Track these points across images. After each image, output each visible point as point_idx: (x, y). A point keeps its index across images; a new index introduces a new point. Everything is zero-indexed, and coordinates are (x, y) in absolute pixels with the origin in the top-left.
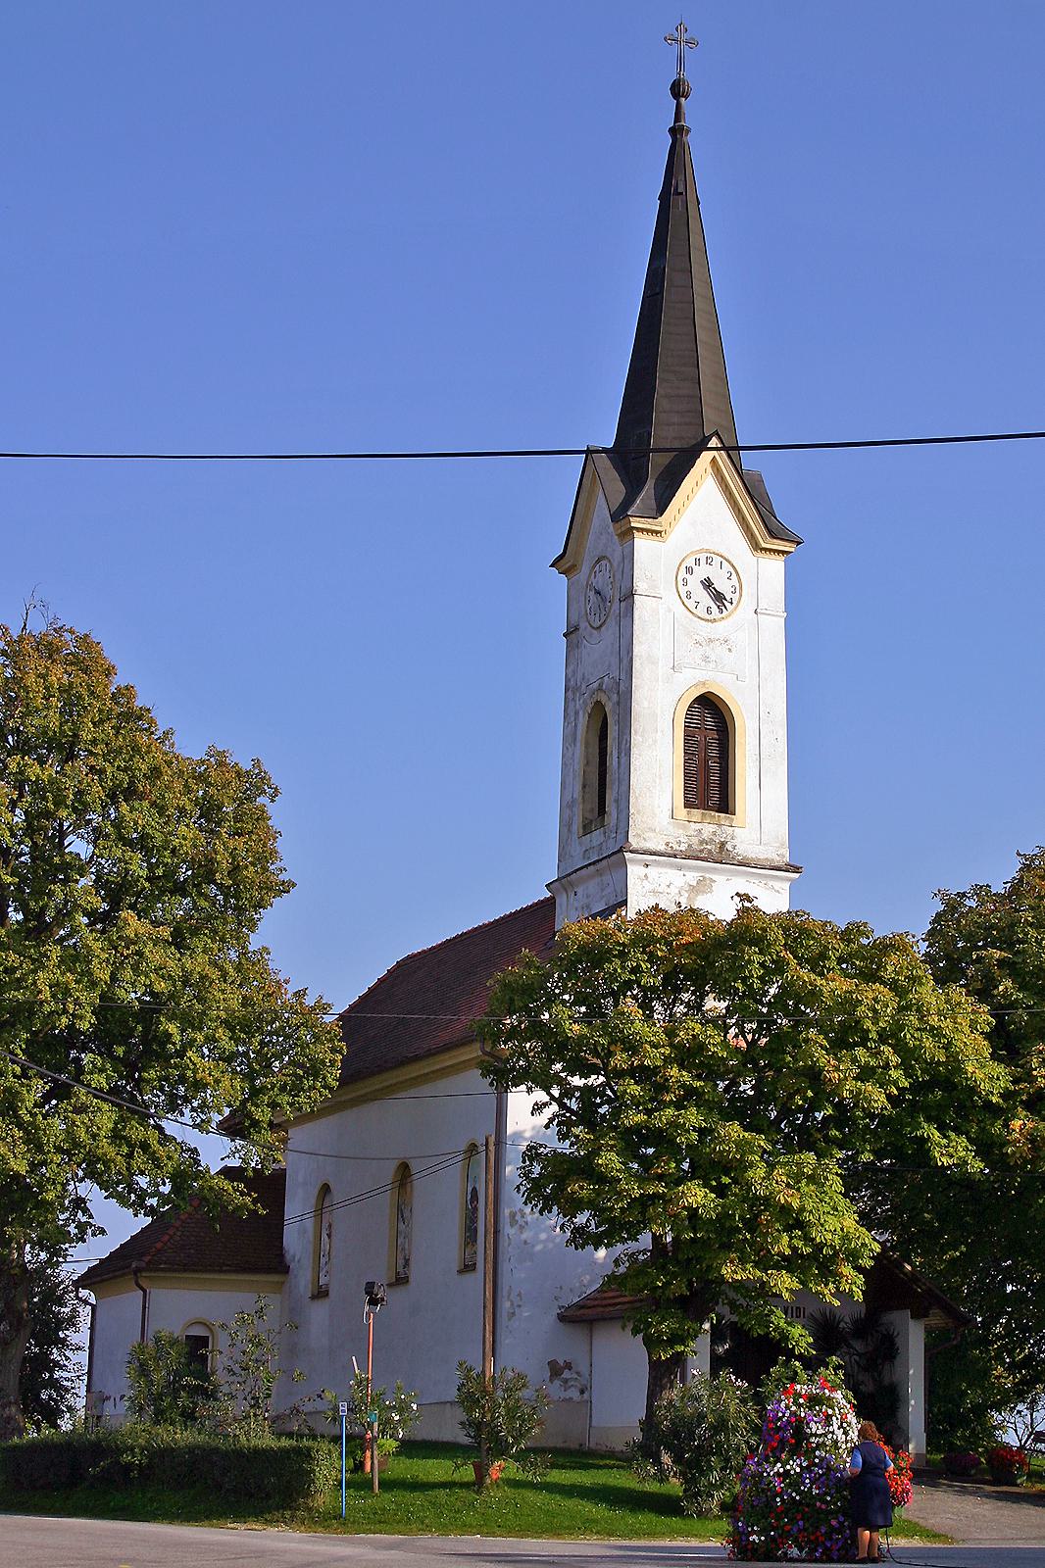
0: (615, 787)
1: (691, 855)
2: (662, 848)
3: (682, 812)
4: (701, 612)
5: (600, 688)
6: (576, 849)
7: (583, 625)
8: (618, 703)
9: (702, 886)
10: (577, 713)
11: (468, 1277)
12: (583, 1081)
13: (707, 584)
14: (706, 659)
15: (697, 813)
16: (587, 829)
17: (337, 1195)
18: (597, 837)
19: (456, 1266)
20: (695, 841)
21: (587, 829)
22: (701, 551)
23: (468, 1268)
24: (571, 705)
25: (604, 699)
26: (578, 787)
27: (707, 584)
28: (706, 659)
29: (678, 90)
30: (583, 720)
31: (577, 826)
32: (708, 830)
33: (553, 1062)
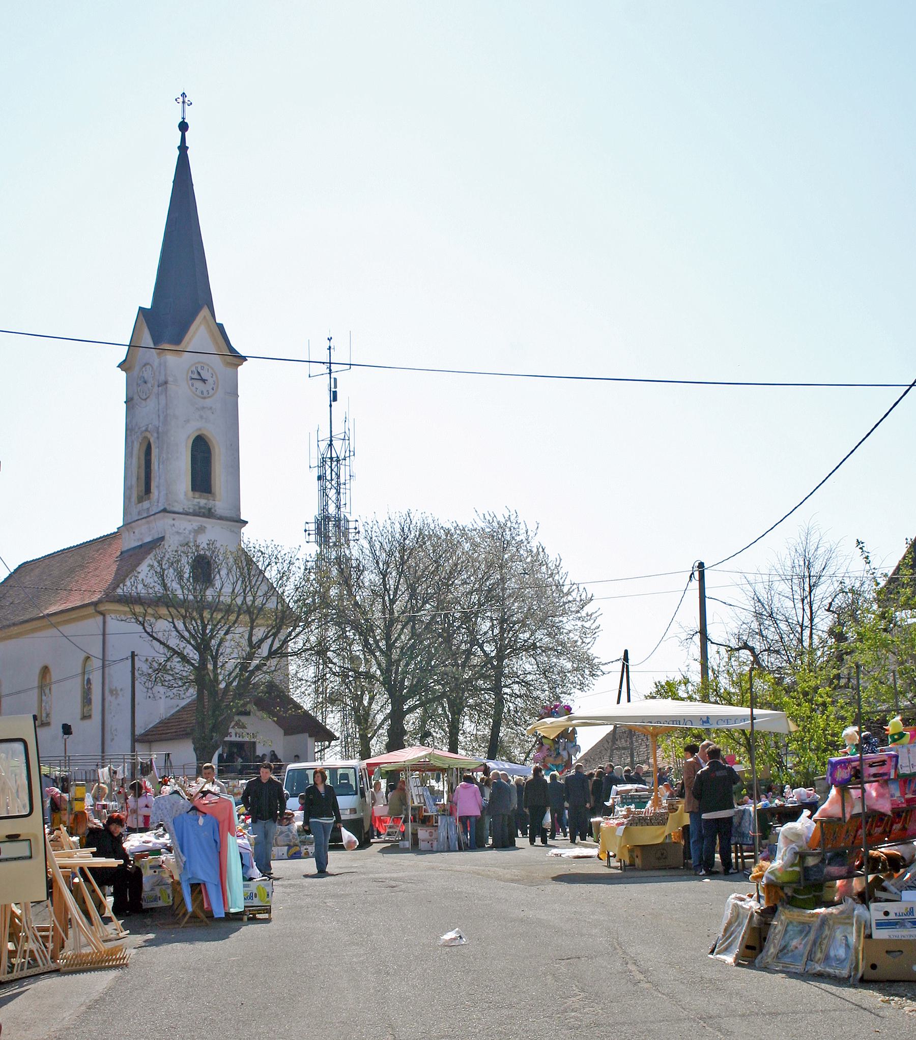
0: (157, 479)
1: (195, 514)
2: (181, 510)
3: (190, 493)
4: (206, 367)
5: (146, 430)
6: (134, 511)
7: (136, 397)
8: (158, 438)
9: (201, 530)
10: (133, 442)
11: (87, 722)
12: (487, 826)
13: (204, 381)
14: (201, 417)
15: (197, 494)
16: (140, 500)
17: (55, 675)
18: (146, 504)
19: (79, 716)
20: (197, 508)
21: (140, 500)
22: (199, 363)
23: (86, 717)
24: (129, 438)
25: (149, 435)
26: (134, 479)
27: (204, 381)
28: (201, 417)
29: (183, 127)
30: (136, 446)
31: (134, 498)
32: (203, 502)
33: (816, 866)
